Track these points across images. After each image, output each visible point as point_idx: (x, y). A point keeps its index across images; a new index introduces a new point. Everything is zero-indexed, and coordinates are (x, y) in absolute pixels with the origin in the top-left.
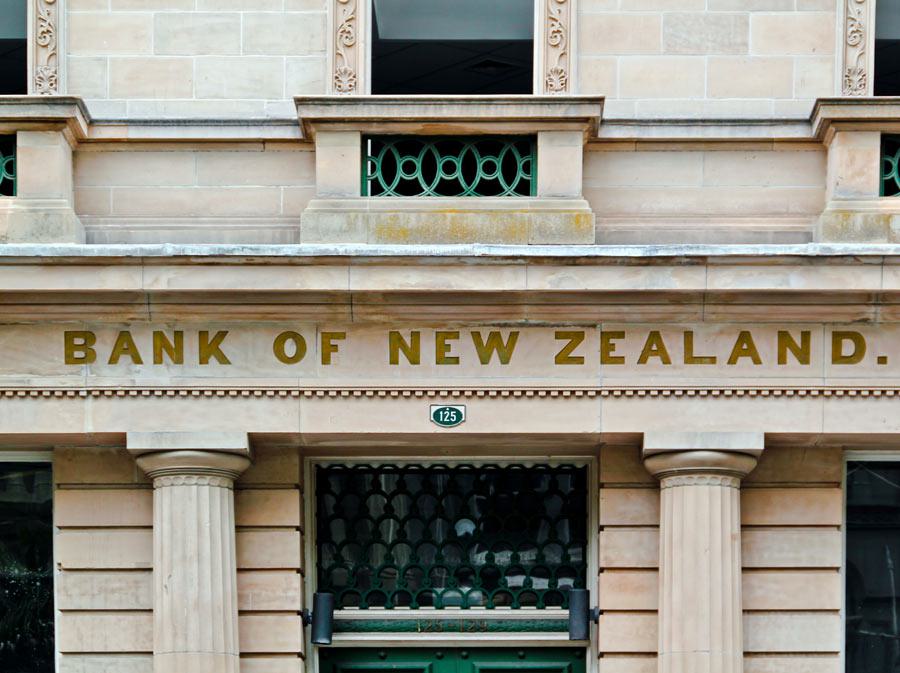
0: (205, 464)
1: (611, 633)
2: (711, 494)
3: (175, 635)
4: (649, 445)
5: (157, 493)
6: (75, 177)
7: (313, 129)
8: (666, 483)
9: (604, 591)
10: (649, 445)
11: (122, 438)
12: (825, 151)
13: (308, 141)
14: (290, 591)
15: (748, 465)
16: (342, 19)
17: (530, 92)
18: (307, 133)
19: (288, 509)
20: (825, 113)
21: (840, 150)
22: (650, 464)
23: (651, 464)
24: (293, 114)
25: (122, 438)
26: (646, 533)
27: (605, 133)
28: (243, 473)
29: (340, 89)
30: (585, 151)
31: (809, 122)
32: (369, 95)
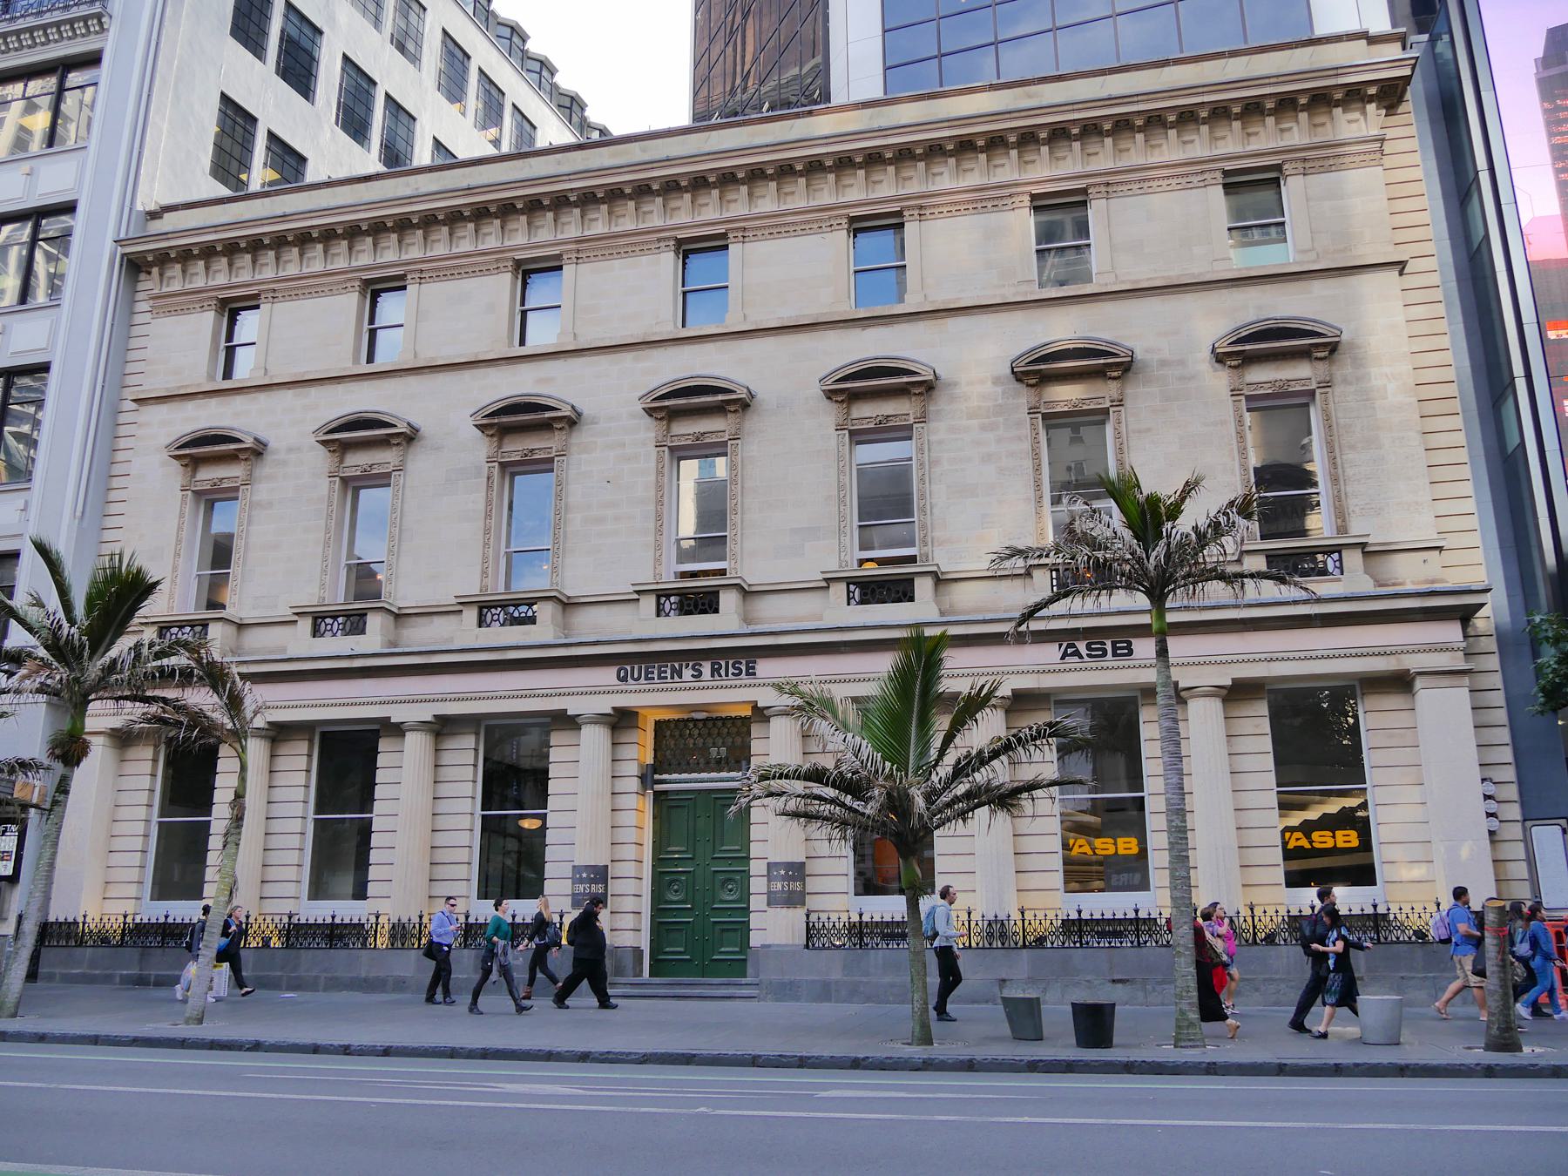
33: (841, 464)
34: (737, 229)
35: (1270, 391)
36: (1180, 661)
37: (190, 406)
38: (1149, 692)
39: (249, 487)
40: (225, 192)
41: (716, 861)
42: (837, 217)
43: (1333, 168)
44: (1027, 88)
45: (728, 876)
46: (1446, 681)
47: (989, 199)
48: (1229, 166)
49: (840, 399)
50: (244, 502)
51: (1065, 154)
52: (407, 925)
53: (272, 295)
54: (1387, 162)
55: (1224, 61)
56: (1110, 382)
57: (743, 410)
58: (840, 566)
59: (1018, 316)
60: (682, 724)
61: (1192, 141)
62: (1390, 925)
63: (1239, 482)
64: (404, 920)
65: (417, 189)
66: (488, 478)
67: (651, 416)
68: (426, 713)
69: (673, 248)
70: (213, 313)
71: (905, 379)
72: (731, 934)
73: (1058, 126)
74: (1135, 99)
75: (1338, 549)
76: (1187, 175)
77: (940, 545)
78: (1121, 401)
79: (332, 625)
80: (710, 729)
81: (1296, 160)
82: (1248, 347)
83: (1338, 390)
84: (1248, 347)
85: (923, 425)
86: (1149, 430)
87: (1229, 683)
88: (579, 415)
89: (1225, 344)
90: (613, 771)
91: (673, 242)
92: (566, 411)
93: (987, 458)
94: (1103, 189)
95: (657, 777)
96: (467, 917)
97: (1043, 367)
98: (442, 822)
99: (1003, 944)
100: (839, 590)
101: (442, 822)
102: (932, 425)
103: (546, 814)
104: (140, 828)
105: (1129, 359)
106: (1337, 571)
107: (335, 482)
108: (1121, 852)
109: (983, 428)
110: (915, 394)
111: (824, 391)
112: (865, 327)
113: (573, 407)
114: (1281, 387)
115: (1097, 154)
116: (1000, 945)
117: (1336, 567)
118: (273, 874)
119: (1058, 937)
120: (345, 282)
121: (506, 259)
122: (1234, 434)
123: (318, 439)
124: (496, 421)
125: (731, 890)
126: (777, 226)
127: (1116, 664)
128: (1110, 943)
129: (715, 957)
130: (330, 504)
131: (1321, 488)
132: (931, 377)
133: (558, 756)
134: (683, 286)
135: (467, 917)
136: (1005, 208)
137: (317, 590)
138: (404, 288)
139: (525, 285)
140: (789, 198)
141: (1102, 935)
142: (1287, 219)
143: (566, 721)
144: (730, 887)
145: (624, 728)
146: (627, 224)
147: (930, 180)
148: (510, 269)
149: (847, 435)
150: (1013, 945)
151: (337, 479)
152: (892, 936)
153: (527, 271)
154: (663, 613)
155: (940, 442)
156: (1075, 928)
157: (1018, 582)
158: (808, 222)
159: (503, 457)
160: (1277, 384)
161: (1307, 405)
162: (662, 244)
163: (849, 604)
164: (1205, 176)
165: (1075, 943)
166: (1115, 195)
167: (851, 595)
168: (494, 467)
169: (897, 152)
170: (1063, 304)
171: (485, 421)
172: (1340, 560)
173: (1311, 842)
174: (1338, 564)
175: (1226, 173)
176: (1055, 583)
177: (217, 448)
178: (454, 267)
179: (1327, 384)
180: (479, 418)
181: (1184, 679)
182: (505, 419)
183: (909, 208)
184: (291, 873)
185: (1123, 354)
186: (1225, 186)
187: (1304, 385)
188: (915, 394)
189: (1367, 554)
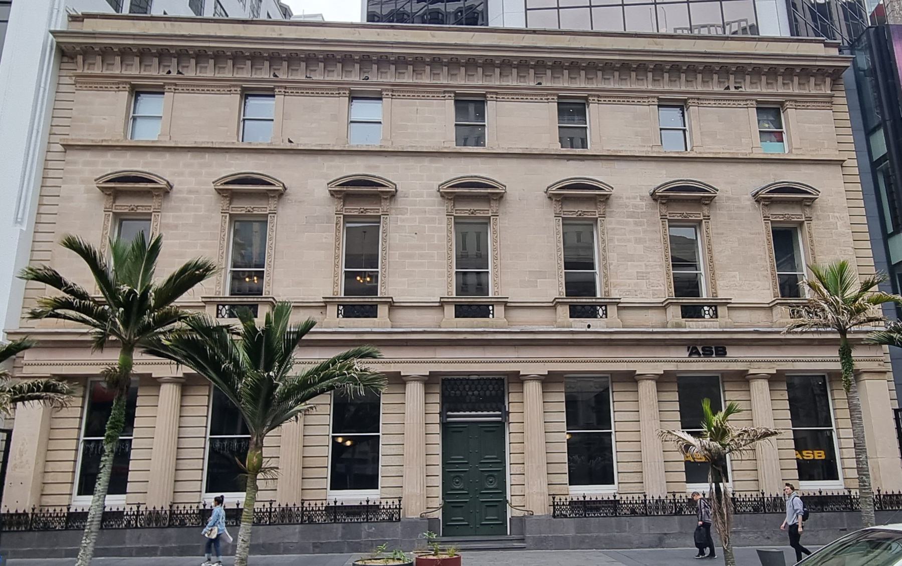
0: (174, 381)
1: (512, 418)
2: (170, 387)
3: (410, 419)
4: (521, 373)
5: (407, 385)
6: (389, 314)
7: (444, 304)
8: (750, 381)
9: (512, 408)
10: (521, 373)
11: (400, 372)
12: (556, 309)
13: (326, 306)
14: (437, 408)
15: (543, 378)
16: (449, 280)
17: (377, 295)
18: (442, 305)
19: (438, 389)
20: (557, 300)
21: (560, 308)
22: (521, 378)
23: (637, 377)
24: (322, 300)
25: (400, 372)
26: (521, 394)
27: (509, 304)
28: (427, 381)
29: (448, 295)
30: (505, 309)
31: (552, 302)
32: (455, 296)
33: (105, 232)
34: (594, 96)
35: (782, 219)
36: (138, 362)
37: (109, 156)
38: (834, 375)
39: (276, 215)
40: (111, 11)
41: (449, 466)
42: (551, 94)
43: (809, 108)
44: (655, 39)
45: (490, 473)
46: (876, 376)
47: (538, 94)
48: (760, 99)
49: (108, 193)
50: (155, 224)
51: (576, 76)
52: (293, 509)
53: (174, 87)
54: (835, 108)
55: (755, 43)
56: (703, 206)
57: (164, 196)
58: (334, 294)
59: (652, 166)
60: (495, 381)
61: (404, 73)
62: (858, 501)
63: (769, 266)
64: (291, 505)
65: (280, 35)
66: (337, 224)
67: (103, 192)
68: (424, 370)
69: (239, 92)
70: (127, 93)
71: (489, 191)
72: (459, 510)
73: (471, 57)
74: (718, 56)
75: (606, 305)
76: (738, 100)
77: (614, 287)
78: (709, 216)
79: (709, 311)
80: (464, 385)
81: (792, 101)
82: (775, 196)
83: (392, 217)
84: (775, 196)
85: (603, 219)
86: (723, 234)
87: (428, 374)
88: (285, 189)
89: (764, 193)
90: (426, 410)
91: (129, 86)
92: (163, 184)
93: (638, 241)
94: (696, 101)
95: (449, 413)
96: (68, 509)
97: (456, 191)
98: (310, 441)
99: (664, 513)
100: (332, 310)
101: (310, 441)
102: (607, 219)
103: (131, 440)
104: (72, 444)
105: (504, 191)
106: (604, 316)
107: (226, 216)
108: (817, 458)
109: (636, 224)
110: (600, 201)
111: (330, 191)
112: (568, 160)
113: (168, 182)
114: (788, 218)
115: (473, 75)
116: (662, 513)
117: (221, 311)
118: (183, 475)
119: (322, 517)
120: (230, 87)
121: (345, 89)
122: (766, 240)
123: (216, 187)
124: (345, 189)
125: (491, 482)
126: (516, 94)
127: (717, 359)
128: (351, 520)
129: (483, 523)
130: (223, 230)
131: (597, 270)
132: (394, 190)
133: (387, 400)
134: (244, 116)
135: (68, 509)
136: (644, 104)
137: (213, 286)
138: (163, 93)
139: (136, 101)
140: (258, 72)
141: (348, 515)
142: (588, 125)
143: (518, 379)
144: (491, 480)
145: (775, 381)
146: (335, 77)
147: (484, 78)
148: (128, 89)
149: (228, 217)
150: (296, 522)
151: (111, 213)
152: (591, 509)
153: (137, 92)
154: (220, 316)
155: (613, 229)
156: (334, 511)
157: (319, 311)
158: (535, 95)
159: (232, 211)
160: (786, 216)
161: (592, 225)
162: (447, 95)
163: (338, 317)
164: (748, 102)
165: (331, 520)
166: (702, 105)
167: (219, 312)
168: (340, 217)
169: (362, 57)
170: (200, 152)
171: (337, 189)
172: (606, 310)
173: (802, 456)
174: (604, 312)
175: (559, 97)
176: (491, 312)
177: (137, 185)
178: (309, 89)
179: (809, 219)
180: (219, 184)
181: (858, 365)
182: (351, 189)
183: (491, 93)
184: (197, 475)
185: (501, 188)
186: (757, 108)
187: (798, 218)
188: (271, 197)
189: (619, 308)
